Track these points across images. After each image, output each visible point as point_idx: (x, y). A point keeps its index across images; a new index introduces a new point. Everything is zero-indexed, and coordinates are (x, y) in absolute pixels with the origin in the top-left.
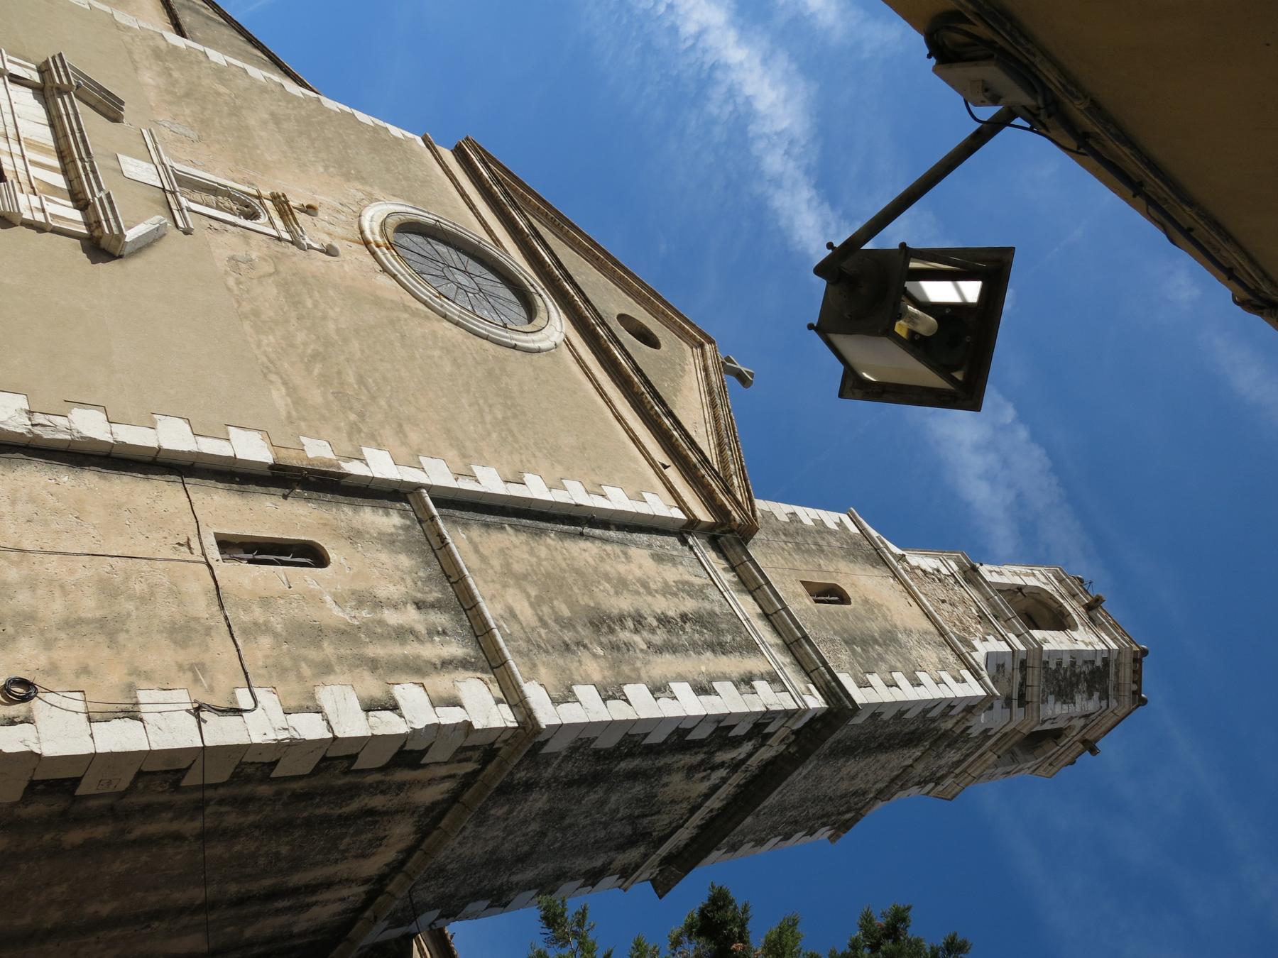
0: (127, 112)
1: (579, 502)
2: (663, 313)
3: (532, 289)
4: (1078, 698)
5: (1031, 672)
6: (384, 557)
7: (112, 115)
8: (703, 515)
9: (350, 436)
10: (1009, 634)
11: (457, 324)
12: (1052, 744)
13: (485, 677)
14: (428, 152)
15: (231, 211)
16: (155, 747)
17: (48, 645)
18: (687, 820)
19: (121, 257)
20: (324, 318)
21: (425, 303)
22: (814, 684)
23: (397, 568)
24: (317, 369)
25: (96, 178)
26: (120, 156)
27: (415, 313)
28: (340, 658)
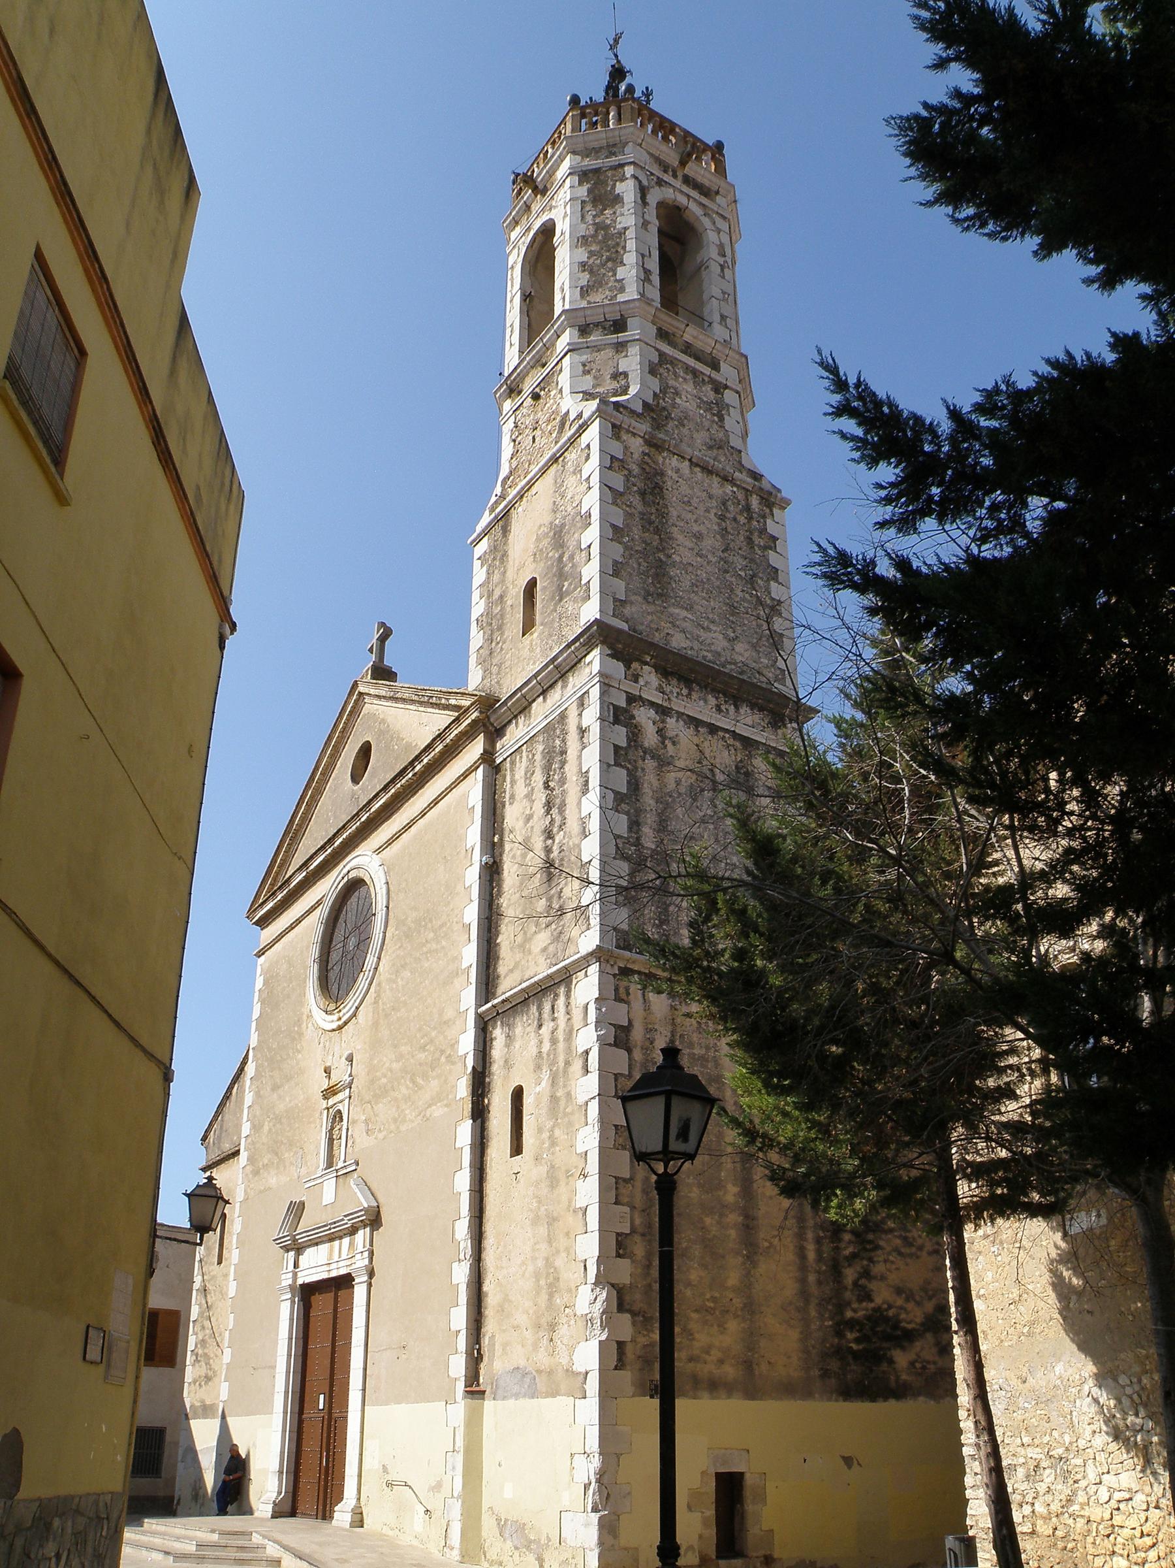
2: (342, 732)
3: (346, 879)
6: (517, 1044)
8: (477, 747)
9: (454, 1063)
10: (558, 351)
13: (574, 982)
17: (558, 1252)
18: (727, 731)
19: (378, 1207)
20: (391, 1070)
21: (370, 984)
22: (585, 656)
23: (522, 1036)
24: (420, 1081)
25: (338, 1221)
26: (324, 1204)
27: (378, 996)
28: (565, 1086)
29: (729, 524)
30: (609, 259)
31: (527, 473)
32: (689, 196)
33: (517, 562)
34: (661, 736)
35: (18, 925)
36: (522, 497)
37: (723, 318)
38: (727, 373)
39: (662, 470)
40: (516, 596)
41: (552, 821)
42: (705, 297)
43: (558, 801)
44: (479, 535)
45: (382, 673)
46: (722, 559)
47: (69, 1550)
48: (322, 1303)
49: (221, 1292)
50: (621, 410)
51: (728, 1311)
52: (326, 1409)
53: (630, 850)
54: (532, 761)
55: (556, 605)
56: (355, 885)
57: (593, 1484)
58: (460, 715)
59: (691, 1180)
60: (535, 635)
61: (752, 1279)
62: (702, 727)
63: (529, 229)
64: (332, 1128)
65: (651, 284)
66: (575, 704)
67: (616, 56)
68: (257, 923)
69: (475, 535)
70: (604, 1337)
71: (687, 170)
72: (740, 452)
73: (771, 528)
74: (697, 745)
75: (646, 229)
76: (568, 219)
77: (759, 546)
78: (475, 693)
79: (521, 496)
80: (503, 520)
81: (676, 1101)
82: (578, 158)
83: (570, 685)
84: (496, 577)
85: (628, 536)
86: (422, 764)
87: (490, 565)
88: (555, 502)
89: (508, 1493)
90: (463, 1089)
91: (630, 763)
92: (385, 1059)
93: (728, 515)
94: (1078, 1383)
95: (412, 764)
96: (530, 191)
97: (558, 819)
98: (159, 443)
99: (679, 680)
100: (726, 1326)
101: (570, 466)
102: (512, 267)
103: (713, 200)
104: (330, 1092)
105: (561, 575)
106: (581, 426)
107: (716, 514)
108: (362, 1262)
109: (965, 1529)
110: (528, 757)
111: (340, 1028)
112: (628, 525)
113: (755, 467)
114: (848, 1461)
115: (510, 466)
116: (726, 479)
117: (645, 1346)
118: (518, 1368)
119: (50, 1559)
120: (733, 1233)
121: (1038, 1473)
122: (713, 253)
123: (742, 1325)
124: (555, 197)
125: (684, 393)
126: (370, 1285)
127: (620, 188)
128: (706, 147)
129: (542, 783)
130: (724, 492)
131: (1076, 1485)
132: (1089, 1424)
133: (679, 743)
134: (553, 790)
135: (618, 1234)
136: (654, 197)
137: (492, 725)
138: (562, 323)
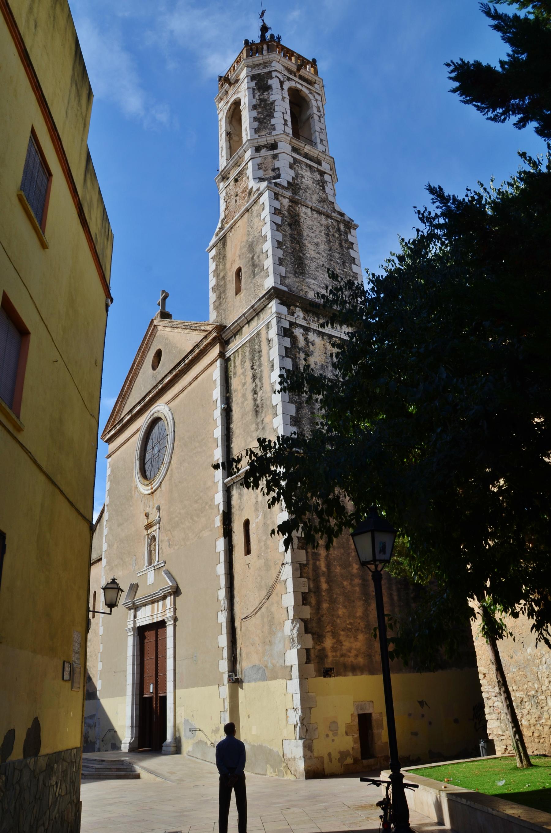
0: (134, 582)
1: (220, 414)
3: (152, 418)
4: (272, 98)
5: (260, 143)
7: (136, 587)
8: (216, 350)
9: (213, 509)
11: (171, 457)
12: (302, 92)
14: (113, 456)
15: (155, 545)
16: (292, 576)
19: (177, 584)
21: (167, 470)
22: (268, 304)
23: (247, 494)
24: (196, 519)
25: (156, 593)
26: (148, 584)
27: (171, 476)
29: (331, 238)
30: (267, 115)
31: (234, 217)
32: (302, 85)
33: (231, 260)
34: (306, 341)
35: (31, 458)
36: (232, 228)
37: (321, 141)
38: (325, 167)
39: (298, 213)
40: (231, 276)
41: (256, 386)
42: (312, 132)
43: (258, 376)
44: (211, 247)
45: (165, 315)
46: (328, 254)
47: (61, 780)
48: (150, 636)
49: (95, 633)
50: (278, 186)
51: (358, 629)
52: (154, 692)
53: (296, 398)
54: (244, 356)
55: (252, 280)
56: (156, 421)
57: (299, 725)
58: (207, 335)
59: (335, 563)
60: (242, 295)
61: (368, 612)
62: (325, 336)
63: (228, 102)
64: (150, 545)
65: (288, 126)
66: (264, 328)
67: (263, 21)
68: (107, 441)
69: (208, 248)
70: (299, 647)
71: (300, 73)
72: (333, 203)
73: (350, 239)
74: (324, 345)
75: (284, 101)
76: (247, 97)
77: (345, 248)
78: (214, 324)
79: (231, 228)
80: (223, 240)
81: (377, 534)
82: (250, 69)
83: (261, 318)
84: (221, 267)
85: (285, 245)
86: (189, 359)
87: (217, 262)
88: (248, 231)
89: (254, 732)
90: (218, 522)
91: (293, 355)
92: (176, 508)
93: (330, 233)
94: (540, 657)
95: (183, 359)
96: (228, 85)
97: (259, 384)
98: (81, 215)
99: (313, 314)
100: (358, 637)
101: (255, 213)
102: (221, 120)
103: (313, 86)
104: (149, 526)
105: (254, 266)
106: (259, 194)
107: (324, 233)
108: (170, 614)
109: (487, 735)
110: (242, 354)
111: (152, 493)
112: (284, 240)
113: (341, 210)
114: (421, 703)
115: (225, 214)
116: (328, 216)
117: (320, 650)
118: (255, 665)
119: (54, 786)
120: (357, 589)
121: (522, 704)
122: (315, 110)
123: (366, 636)
124: (240, 87)
125: (306, 177)
126: (175, 626)
127: (270, 82)
128: (308, 62)
129: (250, 366)
130: (328, 223)
131: (542, 709)
132: (547, 678)
133: (315, 344)
134: (255, 370)
135: (303, 593)
136: (286, 85)
137: (223, 339)
138: (247, 146)
